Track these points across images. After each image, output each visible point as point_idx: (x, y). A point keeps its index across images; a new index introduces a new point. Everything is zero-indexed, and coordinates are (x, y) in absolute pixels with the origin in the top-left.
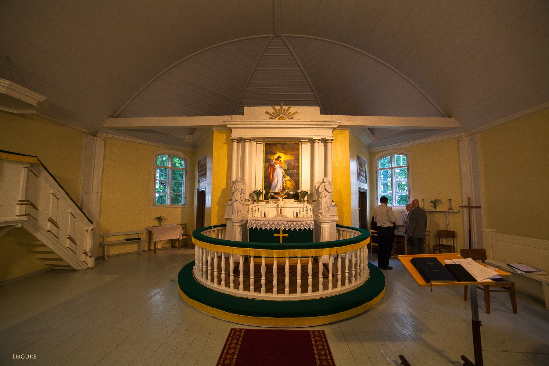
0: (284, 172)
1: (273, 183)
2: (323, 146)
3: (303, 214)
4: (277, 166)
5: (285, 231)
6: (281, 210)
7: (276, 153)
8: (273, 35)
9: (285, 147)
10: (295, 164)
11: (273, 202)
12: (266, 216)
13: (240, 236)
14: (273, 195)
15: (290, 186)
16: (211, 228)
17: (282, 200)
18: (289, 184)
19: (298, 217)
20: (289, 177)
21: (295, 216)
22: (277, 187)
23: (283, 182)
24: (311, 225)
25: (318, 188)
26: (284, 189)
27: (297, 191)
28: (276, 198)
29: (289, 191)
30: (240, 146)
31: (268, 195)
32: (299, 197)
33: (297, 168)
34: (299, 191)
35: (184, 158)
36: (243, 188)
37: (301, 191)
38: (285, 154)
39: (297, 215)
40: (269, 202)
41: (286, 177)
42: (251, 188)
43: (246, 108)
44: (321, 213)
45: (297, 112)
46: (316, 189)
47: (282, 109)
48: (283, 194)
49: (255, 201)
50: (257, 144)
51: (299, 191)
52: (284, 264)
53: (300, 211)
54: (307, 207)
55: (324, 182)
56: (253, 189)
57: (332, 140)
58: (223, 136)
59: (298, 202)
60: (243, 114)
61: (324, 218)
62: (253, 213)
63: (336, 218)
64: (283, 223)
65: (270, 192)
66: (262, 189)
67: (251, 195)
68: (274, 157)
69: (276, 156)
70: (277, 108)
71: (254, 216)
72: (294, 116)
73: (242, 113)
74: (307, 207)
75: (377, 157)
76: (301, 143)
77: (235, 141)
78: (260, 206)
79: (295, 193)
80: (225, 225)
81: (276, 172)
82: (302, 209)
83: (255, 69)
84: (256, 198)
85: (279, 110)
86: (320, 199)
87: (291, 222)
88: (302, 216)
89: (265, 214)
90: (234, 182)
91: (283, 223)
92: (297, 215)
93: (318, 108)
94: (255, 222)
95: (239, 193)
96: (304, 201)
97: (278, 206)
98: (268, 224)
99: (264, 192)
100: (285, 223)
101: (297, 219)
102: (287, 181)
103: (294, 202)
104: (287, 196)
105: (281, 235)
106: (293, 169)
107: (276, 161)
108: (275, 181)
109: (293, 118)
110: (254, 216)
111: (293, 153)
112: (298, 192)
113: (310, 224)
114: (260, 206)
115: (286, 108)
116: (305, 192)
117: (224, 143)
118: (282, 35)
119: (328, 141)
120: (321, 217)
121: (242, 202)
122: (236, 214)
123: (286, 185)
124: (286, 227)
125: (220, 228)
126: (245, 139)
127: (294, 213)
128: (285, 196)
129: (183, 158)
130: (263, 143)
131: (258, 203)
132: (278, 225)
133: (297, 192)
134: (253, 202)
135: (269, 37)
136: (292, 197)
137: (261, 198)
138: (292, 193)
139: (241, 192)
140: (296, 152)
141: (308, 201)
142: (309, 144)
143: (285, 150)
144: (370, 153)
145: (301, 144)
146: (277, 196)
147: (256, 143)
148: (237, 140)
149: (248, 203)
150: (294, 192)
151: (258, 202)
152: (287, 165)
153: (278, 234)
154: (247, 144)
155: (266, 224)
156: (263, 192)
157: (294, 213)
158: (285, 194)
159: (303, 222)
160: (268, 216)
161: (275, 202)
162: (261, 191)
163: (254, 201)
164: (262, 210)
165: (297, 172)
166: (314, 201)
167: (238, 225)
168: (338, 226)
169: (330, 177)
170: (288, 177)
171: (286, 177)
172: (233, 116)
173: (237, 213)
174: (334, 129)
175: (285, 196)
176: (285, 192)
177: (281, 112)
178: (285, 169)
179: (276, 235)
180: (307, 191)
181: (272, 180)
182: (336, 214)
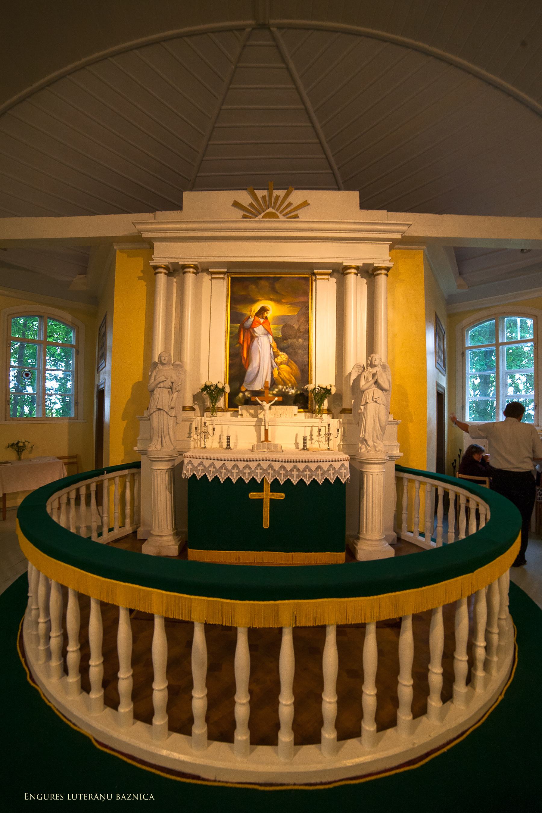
0: (274, 344)
1: (250, 370)
2: (366, 286)
3: (319, 441)
4: (259, 330)
5: (275, 486)
6: (266, 431)
7: (257, 301)
8: (251, 22)
9: (277, 285)
10: (300, 326)
11: (248, 412)
12: (232, 446)
13: (168, 493)
14: (249, 396)
15: (287, 377)
16: (103, 474)
17: (270, 408)
18: (285, 371)
19: (308, 450)
20: (287, 356)
21: (301, 446)
22: (259, 378)
23: (272, 366)
24: (343, 471)
25: (357, 380)
26: (274, 383)
27: (306, 387)
28: (256, 403)
29: (287, 388)
30: (175, 285)
31: (237, 398)
32: (310, 402)
33: (306, 334)
34: (311, 387)
35: (72, 323)
36: (175, 378)
37: (315, 388)
38: (278, 301)
39: (305, 443)
40: (240, 412)
41: (279, 355)
42: (199, 379)
43: (187, 196)
44: (366, 440)
45: (305, 204)
46: (352, 382)
47: (270, 195)
48: (273, 394)
49: (206, 410)
50: (212, 278)
51: (311, 387)
52: (276, 209)
53: (311, 435)
54: (329, 425)
55: (372, 366)
56: (204, 381)
57: (388, 269)
58: (138, 263)
59: (308, 414)
60: (182, 210)
61: (372, 452)
62: (201, 437)
63: (397, 452)
64: (271, 466)
65: (243, 389)
66: (223, 382)
67: (196, 397)
68: (253, 310)
69: (256, 307)
70: (260, 193)
71: (202, 446)
72: (299, 212)
73: (179, 207)
74: (329, 425)
75: (465, 322)
76: (314, 278)
77: (163, 270)
78: (219, 423)
79: (299, 392)
80: (137, 465)
81: (255, 343)
82: (315, 430)
83: (214, 127)
84: (208, 403)
85: (264, 197)
86: (362, 407)
87: (292, 465)
88: (316, 445)
89: (228, 442)
90: (156, 364)
91: (271, 466)
92: (305, 443)
93: (355, 196)
94: (201, 462)
95: (166, 391)
96: (320, 412)
97: (260, 421)
98: (233, 468)
99: (228, 390)
100: (277, 466)
101: (305, 456)
102: (281, 363)
103: (299, 412)
104: (281, 399)
105: (267, 495)
106: (295, 338)
107: (256, 317)
108: (255, 364)
109: (296, 217)
110: (202, 446)
111: (297, 300)
112: (306, 390)
113: (340, 468)
114: (219, 423)
115: (281, 193)
116: (323, 389)
117: (140, 278)
118: (273, 21)
119: (379, 272)
120: (365, 449)
121: (173, 413)
122: (160, 443)
123: (279, 374)
124: (280, 475)
125: (126, 472)
126: (184, 267)
127: (296, 440)
128: (276, 399)
129: (70, 324)
130: (226, 278)
131: (213, 415)
132: (259, 471)
133: (303, 390)
134: (202, 411)
135: (241, 29)
136: (292, 402)
137: (221, 403)
138: (292, 392)
139: (171, 388)
140: (303, 299)
141: (329, 411)
142: (333, 280)
143: (277, 292)
144: (450, 316)
145: (315, 280)
146: (257, 398)
147: (210, 277)
148: (167, 268)
149: (190, 414)
150: (298, 389)
151: (213, 412)
152: (283, 327)
153: (260, 492)
154: (190, 278)
155: (229, 468)
156: (224, 388)
157: (296, 440)
158: (276, 395)
159: (321, 464)
160: (235, 446)
161: (252, 412)
162: (220, 386)
163: (204, 410)
164: (222, 432)
165: (306, 343)
166: (344, 411)
167: (163, 467)
168: (399, 468)
169: (381, 356)
170: (283, 356)
171: (279, 355)
172: (158, 213)
173: (160, 439)
174: (394, 244)
175: (276, 399)
176: (276, 390)
177: (268, 202)
178: (277, 337)
179: (253, 495)
180: (329, 388)
181: (246, 362)
182: (396, 443)
